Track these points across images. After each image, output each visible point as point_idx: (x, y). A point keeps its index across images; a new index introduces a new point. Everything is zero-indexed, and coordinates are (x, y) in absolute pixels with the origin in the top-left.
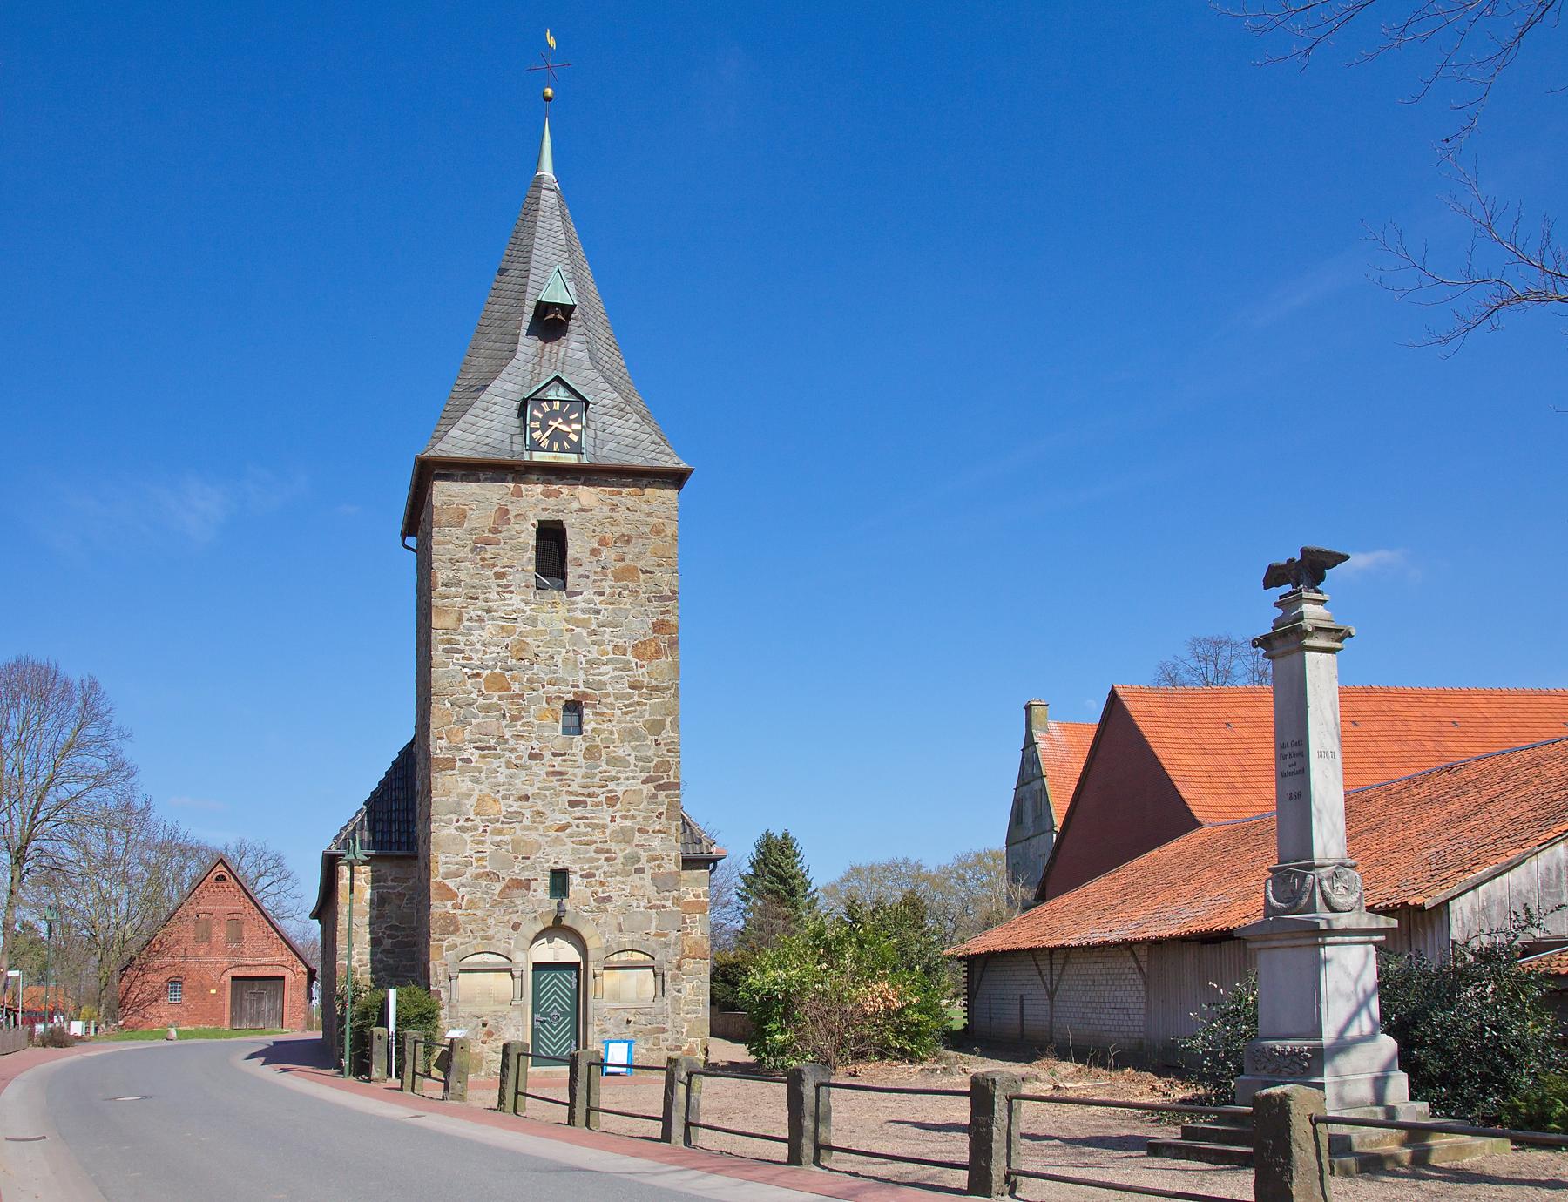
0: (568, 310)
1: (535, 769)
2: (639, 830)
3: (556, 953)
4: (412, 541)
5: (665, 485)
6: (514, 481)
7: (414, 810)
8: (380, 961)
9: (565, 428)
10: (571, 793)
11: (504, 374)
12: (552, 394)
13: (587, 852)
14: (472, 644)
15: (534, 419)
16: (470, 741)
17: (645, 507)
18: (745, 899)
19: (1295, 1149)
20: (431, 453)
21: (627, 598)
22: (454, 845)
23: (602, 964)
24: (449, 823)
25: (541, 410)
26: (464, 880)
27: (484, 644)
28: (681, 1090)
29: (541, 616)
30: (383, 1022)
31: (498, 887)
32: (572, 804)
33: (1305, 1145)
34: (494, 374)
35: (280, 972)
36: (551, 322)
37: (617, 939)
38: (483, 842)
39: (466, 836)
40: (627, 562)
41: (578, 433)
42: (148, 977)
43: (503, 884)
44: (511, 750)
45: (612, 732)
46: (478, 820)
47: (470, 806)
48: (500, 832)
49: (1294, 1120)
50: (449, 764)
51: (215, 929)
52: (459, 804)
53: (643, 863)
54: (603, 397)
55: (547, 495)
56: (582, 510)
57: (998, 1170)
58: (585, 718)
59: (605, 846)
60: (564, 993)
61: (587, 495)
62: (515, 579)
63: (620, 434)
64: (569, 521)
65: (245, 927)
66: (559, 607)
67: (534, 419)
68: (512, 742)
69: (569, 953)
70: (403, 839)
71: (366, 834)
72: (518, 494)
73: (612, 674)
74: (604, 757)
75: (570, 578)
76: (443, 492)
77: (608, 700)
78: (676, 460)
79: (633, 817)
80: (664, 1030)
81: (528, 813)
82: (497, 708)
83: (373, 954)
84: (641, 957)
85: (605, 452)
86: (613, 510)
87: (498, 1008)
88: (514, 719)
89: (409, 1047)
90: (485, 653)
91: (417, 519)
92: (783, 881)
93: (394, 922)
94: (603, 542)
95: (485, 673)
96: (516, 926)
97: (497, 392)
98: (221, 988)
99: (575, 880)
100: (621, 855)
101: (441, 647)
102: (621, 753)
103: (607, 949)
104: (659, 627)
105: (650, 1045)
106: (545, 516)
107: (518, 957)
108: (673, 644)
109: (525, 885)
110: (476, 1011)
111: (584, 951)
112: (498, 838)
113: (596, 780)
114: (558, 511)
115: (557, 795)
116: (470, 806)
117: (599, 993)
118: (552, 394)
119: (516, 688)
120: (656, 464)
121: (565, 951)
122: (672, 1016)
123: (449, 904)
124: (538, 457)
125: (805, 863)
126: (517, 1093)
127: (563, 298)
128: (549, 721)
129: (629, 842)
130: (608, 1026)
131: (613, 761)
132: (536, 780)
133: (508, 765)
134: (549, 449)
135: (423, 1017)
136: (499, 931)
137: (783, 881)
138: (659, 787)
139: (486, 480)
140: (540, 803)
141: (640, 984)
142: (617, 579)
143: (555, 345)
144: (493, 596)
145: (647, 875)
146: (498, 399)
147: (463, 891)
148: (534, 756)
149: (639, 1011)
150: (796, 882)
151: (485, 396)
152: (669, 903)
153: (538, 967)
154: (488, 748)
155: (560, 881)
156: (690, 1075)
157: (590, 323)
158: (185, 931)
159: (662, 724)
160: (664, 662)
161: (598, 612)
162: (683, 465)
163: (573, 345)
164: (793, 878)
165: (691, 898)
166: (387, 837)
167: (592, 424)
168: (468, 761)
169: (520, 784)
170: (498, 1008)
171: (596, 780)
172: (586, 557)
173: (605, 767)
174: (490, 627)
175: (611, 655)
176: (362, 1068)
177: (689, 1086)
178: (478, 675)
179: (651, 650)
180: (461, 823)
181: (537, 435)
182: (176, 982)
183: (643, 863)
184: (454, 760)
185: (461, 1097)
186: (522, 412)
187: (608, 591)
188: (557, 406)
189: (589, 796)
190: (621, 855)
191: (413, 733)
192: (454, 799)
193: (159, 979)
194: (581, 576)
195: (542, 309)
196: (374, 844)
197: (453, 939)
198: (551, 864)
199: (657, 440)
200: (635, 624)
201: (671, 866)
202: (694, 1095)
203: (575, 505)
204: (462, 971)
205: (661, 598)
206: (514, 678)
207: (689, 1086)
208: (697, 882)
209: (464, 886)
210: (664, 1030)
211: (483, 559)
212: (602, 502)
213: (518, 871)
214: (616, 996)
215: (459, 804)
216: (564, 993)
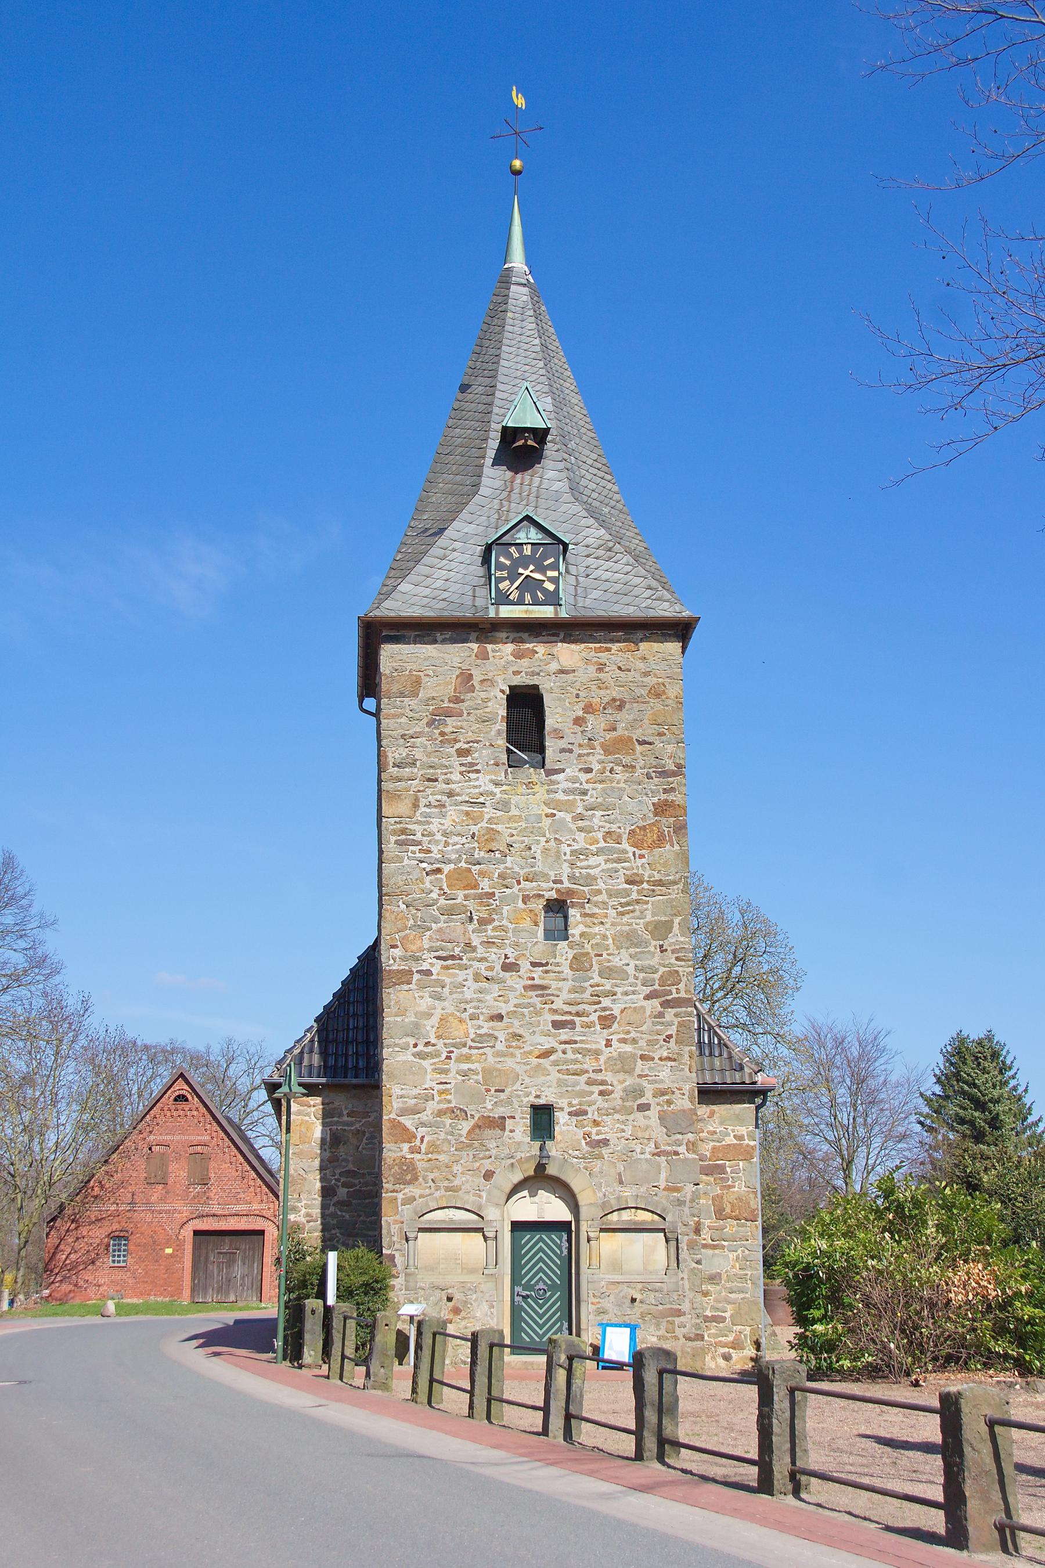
0: (541, 435)
1: (509, 982)
2: (643, 1057)
3: (540, 1210)
4: (370, 703)
5: (664, 638)
6: (478, 640)
8: (334, 1215)
9: (538, 576)
10: (555, 1011)
11: (464, 515)
12: (521, 537)
13: (575, 1084)
14: (431, 834)
15: (500, 567)
16: (431, 950)
17: (641, 665)
18: (931, 1130)
19: (967, 1449)
20: (377, 613)
21: (621, 775)
22: (409, 1074)
23: (597, 1223)
24: (405, 1048)
25: (509, 556)
26: (424, 1117)
27: (445, 834)
28: (561, 1375)
29: (514, 800)
30: (322, 1294)
31: (466, 1126)
32: (556, 1025)
33: (978, 1446)
34: (454, 514)
35: (257, 1224)
36: (521, 450)
37: (615, 1193)
38: (446, 1072)
39: (426, 1063)
40: (620, 732)
41: (555, 581)
42: (84, 1231)
43: (472, 1122)
44: (480, 960)
45: (604, 937)
46: (440, 1044)
47: (430, 1027)
48: (468, 1058)
49: (965, 1419)
50: (405, 977)
51: (173, 1167)
52: (417, 1025)
53: (648, 1098)
54: (585, 535)
55: (518, 655)
56: (562, 672)
57: (781, 1467)
58: (571, 920)
59: (599, 1077)
60: (549, 1261)
62: (482, 756)
63: (603, 578)
64: (547, 686)
65: (212, 1164)
66: (537, 788)
67: (500, 567)
68: (480, 950)
69: (555, 1210)
70: (362, 1064)
71: (316, 1059)
72: (484, 656)
73: (604, 866)
74: (596, 967)
75: (549, 753)
76: (392, 656)
77: (599, 898)
78: (677, 608)
79: (634, 1041)
80: (679, 1313)
81: (501, 1036)
82: (463, 909)
83: (324, 1207)
84: (646, 1216)
85: (588, 602)
86: (600, 670)
87: (467, 1278)
88: (483, 922)
89: (337, 1323)
90: (447, 844)
91: (369, 682)
92: (980, 1105)
93: (351, 1167)
94: (589, 709)
95: (447, 868)
96: (488, 1175)
97: (455, 535)
98: (179, 1246)
99: (562, 1119)
100: (619, 1088)
101: (393, 839)
102: (616, 962)
103: (604, 1205)
104: (661, 809)
105: (662, 1332)
106: (517, 681)
107: (492, 1214)
108: (680, 829)
109: (499, 1123)
110: (440, 1281)
111: (574, 1206)
112: (465, 1066)
113: (587, 995)
114: (533, 674)
115: (538, 1013)
116: (430, 1027)
117: (595, 1262)
118: (521, 537)
119: (485, 885)
120: (652, 613)
121: (551, 1207)
122: (690, 1295)
123: (406, 1147)
124: (507, 612)
125: (1022, 1080)
126: (432, 1380)
127: (534, 421)
128: (527, 923)
129: (630, 1072)
130: (607, 1304)
131: (607, 972)
132: (511, 995)
133: (477, 977)
134: (520, 602)
135: (369, 1290)
136: (467, 1182)
137: (980, 1105)
138: (666, 1004)
139: (444, 641)
140: (516, 1023)
141: (646, 1252)
142: (607, 751)
143: (527, 475)
144: (456, 777)
145: (653, 1113)
146: (457, 545)
147: (422, 1131)
148: (509, 967)
149: (647, 1287)
150: (999, 1108)
151: (442, 541)
152: (682, 1149)
153: (518, 1227)
154: (444, 959)
155: (542, 1119)
156: (570, 1359)
157: (572, 445)
158: (134, 1169)
159: (668, 926)
160: (669, 850)
161: (584, 793)
162: (686, 614)
163: (550, 474)
164: (997, 1101)
165: (731, 1140)
166: (341, 1062)
167: (573, 569)
168: (428, 973)
169: (492, 1002)
170: (467, 1278)
171: (587, 995)
172: (568, 728)
173: (597, 979)
174: (453, 813)
175: (602, 844)
176: (294, 1353)
177: (570, 1371)
178: (439, 871)
179: (651, 837)
180: (420, 1047)
181: (504, 585)
182: (119, 1237)
183: (648, 1098)
184: (410, 972)
185: (385, 1386)
186: (486, 560)
187: (596, 767)
188: (528, 550)
189: (578, 1014)
190: (619, 1088)
192: (411, 1018)
193: (98, 1234)
194: (563, 751)
195: (509, 435)
196: (326, 1069)
197: (409, 1190)
198: (532, 1099)
199: (654, 584)
200: (631, 805)
201: (684, 1102)
202: (576, 1382)
203: (554, 666)
204: (422, 1230)
205: (664, 774)
206: (481, 873)
207: (570, 1371)
208: (739, 1120)
209: (423, 1124)
210: (679, 1313)
211: (442, 734)
212: (587, 661)
213: (490, 1107)
214: (616, 1266)
215: (417, 1025)
216: (549, 1261)
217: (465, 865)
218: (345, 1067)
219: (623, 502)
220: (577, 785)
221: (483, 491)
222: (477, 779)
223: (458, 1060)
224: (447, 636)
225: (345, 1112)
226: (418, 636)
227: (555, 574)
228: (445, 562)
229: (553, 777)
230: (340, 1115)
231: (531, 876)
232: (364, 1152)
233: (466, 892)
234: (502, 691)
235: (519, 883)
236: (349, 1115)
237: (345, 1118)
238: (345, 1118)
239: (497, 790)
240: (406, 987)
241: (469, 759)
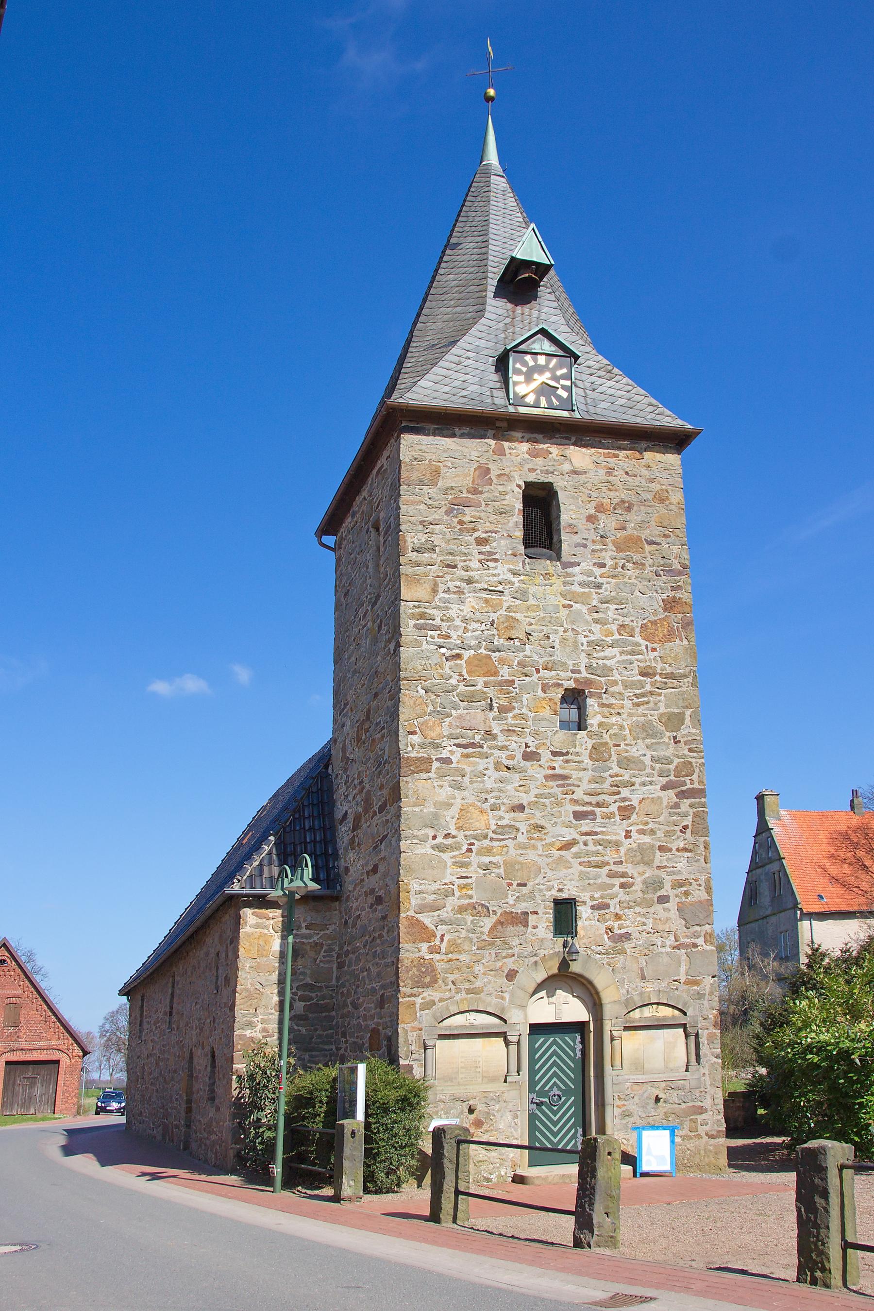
61: (580, 456)
93: (309, 980)
106: (532, 478)
178: (458, 656)
217: (484, 652)
220: (592, 578)
222: (496, 568)
224: (466, 431)
225: (303, 925)
226: (438, 429)
228: (460, 367)
233: (486, 679)
235: (538, 671)
236: (307, 928)
240: (425, 775)
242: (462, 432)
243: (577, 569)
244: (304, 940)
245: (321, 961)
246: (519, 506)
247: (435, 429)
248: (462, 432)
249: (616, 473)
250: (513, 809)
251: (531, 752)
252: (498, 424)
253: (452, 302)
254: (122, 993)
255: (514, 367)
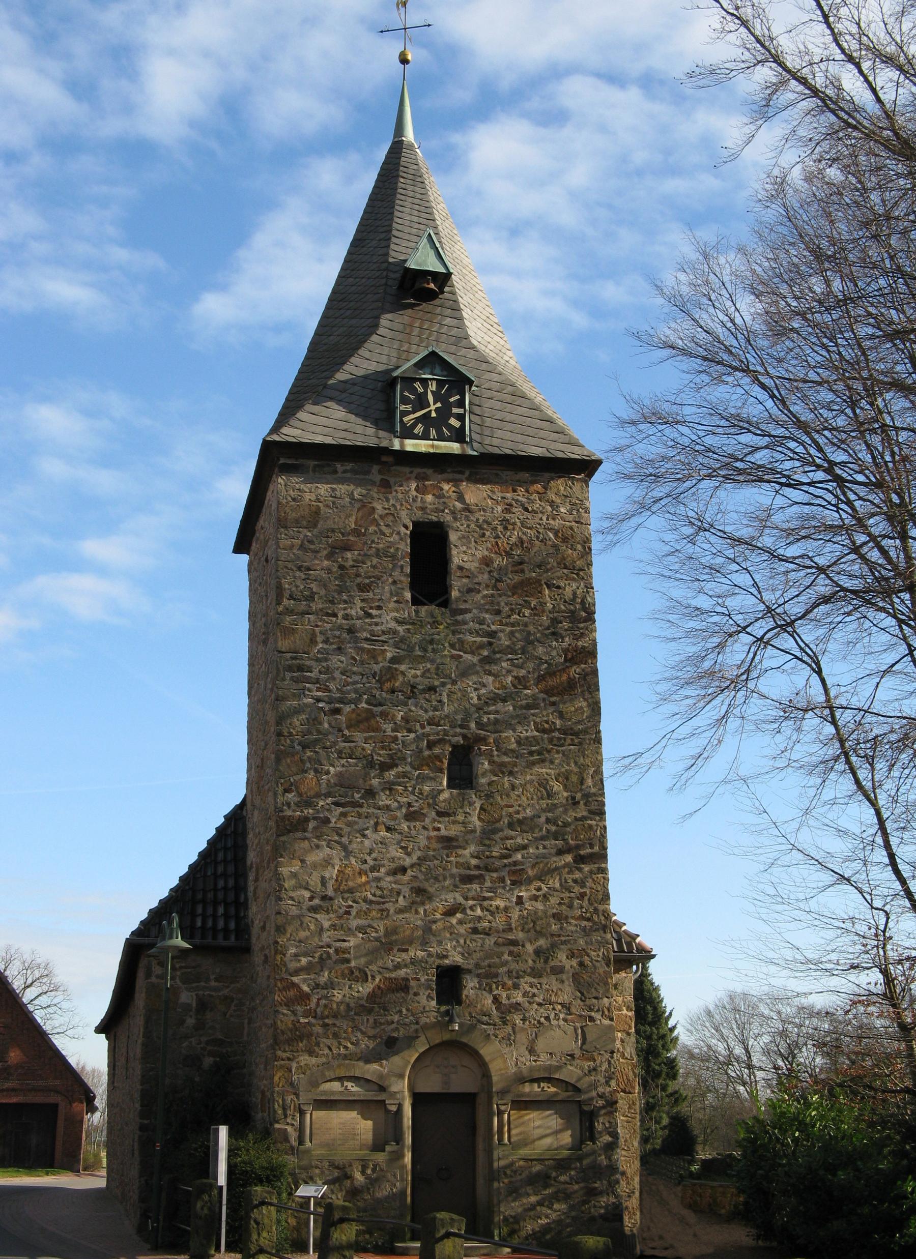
7: (245, 889)
35: (52, 1099)
41: (461, 418)
61: (475, 494)
93: (219, 1036)
106: (419, 515)
134: (425, 436)
178: (337, 711)
191: (244, 792)
217: (365, 706)
218: (214, 929)
219: (514, 358)
220: (485, 627)
221: (381, 331)
222: (380, 616)
223: (358, 915)
224: (348, 468)
225: (212, 977)
226: (318, 466)
227: (461, 411)
228: (344, 395)
229: (460, 618)
230: (208, 980)
231: (437, 720)
232: (232, 1019)
233: (367, 734)
234: (406, 527)
235: (423, 727)
236: (216, 980)
237: (213, 983)
238: (213, 983)
239: (400, 629)
240: (299, 834)
241: (371, 595)
242: (344, 468)
243: (468, 616)
244: (213, 993)
245: (231, 1016)
246: (405, 547)
247: (315, 466)
248: (344, 468)
249: (514, 510)
250: (393, 873)
251: (415, 812)
252: (384, 459)
253: (349, 312)
254: (99, 1030)
255: (402, 395)
